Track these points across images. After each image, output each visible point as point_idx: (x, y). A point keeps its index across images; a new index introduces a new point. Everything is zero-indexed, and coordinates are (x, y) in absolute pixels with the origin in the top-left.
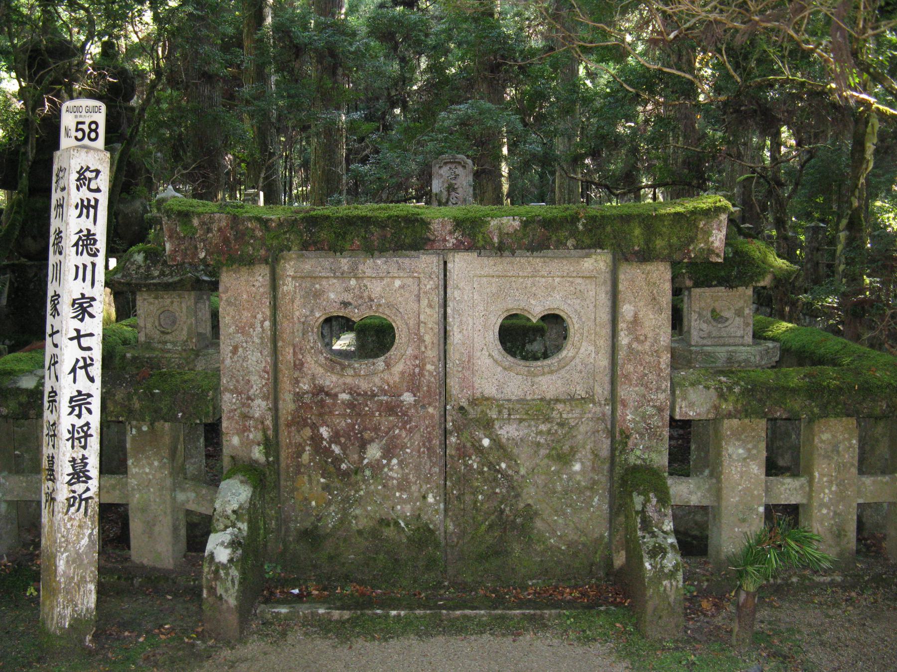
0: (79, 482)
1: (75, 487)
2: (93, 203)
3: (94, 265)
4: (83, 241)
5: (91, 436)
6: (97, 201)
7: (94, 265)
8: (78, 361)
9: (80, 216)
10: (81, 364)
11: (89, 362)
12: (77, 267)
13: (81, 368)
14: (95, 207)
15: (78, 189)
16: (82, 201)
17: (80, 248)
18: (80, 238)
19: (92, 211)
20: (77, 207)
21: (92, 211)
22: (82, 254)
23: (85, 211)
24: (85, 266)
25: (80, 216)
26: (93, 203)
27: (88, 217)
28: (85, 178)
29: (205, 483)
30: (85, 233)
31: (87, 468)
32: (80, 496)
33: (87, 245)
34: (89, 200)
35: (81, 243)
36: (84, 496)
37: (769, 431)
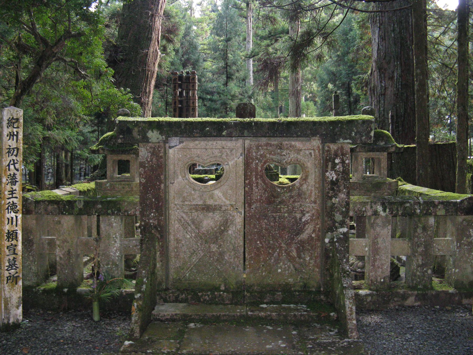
0: (12, 269)
1: (10, 272)
2: (15, 133)
3: (16, 217)
4: (11, 207)
5: (18, 182)
6: (17, 132)
7: (16, 217)
8: (11, 161)
9: (10, 139)
10: (12, 162)
11: (16, 161)
12: (8, 219)
13: (12, 164)
14: (17, 136)
15: (8, 127)
16: (10, 132)
17: (10, 210)
18: (9, 206)
19: (15, 137)
20: (8, 136)
21: (15, 137)
22: (10, 213)
23: (12, 137)
24: (12, 218)
25: (10, 139)
26: (15, 133)
27: (13, 140)
28: (11, 123)
29: (66, 311)
30: (12, 203)
31: (16, 263)
32: (13, 275)
33: (13, 209)
34: (13, 133)
35: (10, 208)
36: (15, 275)
37: (427, 87)
